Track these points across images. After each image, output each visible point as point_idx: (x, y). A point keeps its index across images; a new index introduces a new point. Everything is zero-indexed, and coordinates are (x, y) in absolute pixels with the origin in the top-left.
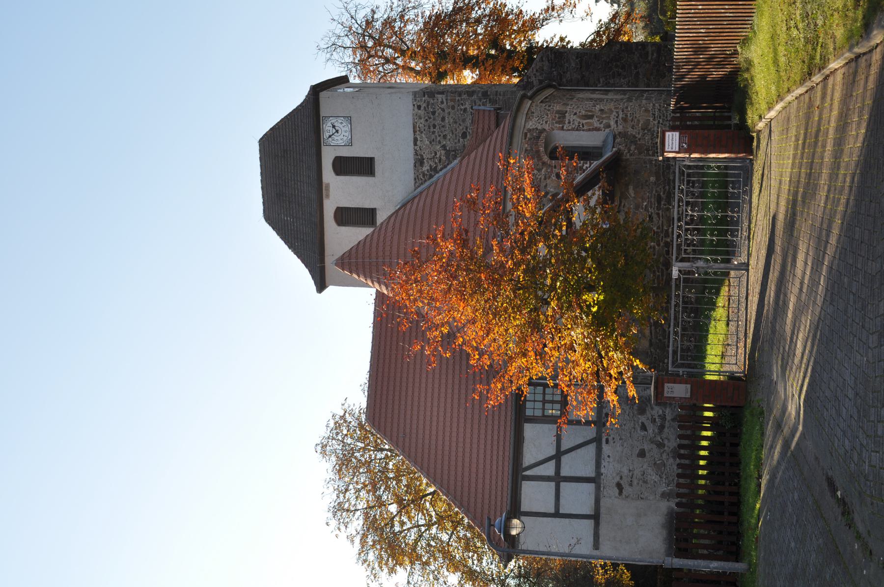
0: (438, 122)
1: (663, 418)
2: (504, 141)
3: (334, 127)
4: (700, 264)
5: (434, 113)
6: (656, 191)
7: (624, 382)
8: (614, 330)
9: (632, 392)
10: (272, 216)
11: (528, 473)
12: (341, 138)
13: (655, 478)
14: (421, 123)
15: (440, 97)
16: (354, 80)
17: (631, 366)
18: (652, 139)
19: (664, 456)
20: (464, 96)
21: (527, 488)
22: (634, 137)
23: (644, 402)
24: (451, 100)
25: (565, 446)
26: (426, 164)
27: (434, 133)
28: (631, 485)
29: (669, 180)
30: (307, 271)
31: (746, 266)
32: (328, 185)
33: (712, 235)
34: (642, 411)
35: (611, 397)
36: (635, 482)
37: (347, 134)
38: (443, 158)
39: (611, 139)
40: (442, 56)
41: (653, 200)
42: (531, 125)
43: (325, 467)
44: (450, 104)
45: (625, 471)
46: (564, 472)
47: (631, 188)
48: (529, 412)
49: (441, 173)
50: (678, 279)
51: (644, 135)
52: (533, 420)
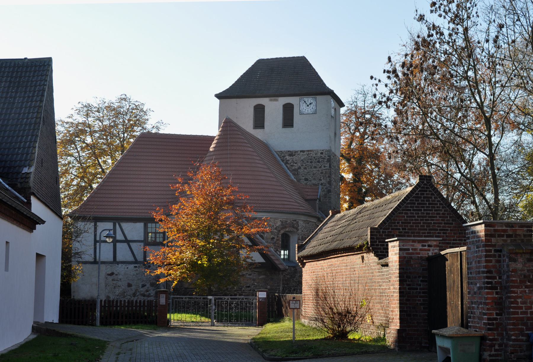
0: (314, 165)
1: (149, 296)
2: (291, 210)
3: (311, 104)
4: (214, 307)
5: (319, 162)
7: (167, 276)
8: (190, 271)
9: (162, 280)
10: (260, 63)
11: (117, 224)
12: (305, 109)
13: (117, 292)
14: (313, 155)
15: (328, 165)
16: (343, 110)
17: (174, 280)
19: (129, 297)
20: (328, 180)
21: (109, 225)
23: (158, 286)
24: (326, 172)
25: (133, 245)
26: (290, 158)
27: (308, 162)
28: (113, 280)
30: (228, 87)
31: (213, 325)
32: (277, 100)
33: (225, 311)
34: (152, 285)
35: (159, 272)
36: (115, 282)
37: (306, 111)
38: (293, 168)
39: (293, 265)
40: (360, 160)
42: (301, 223)
43: (112, 97)
44: (324, 171)
45: (120, 277)
46: (118, 245)
48: (149, 225)
49: (285, 166)
50: (207, 299)
51: (296, 282)
52: (146, 227)
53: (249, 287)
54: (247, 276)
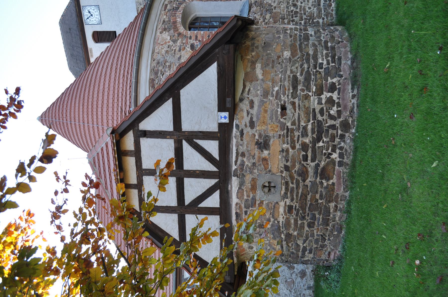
3: (89, 12)
6: (292, 72)
12: (94, 20)
18: (287, 7)
22: (270, 5)
29: (308, 54)
32: (91, 49)
41: (286, 84)
47: (258, 66)
53: (284, 108)
54: (254, 111)
